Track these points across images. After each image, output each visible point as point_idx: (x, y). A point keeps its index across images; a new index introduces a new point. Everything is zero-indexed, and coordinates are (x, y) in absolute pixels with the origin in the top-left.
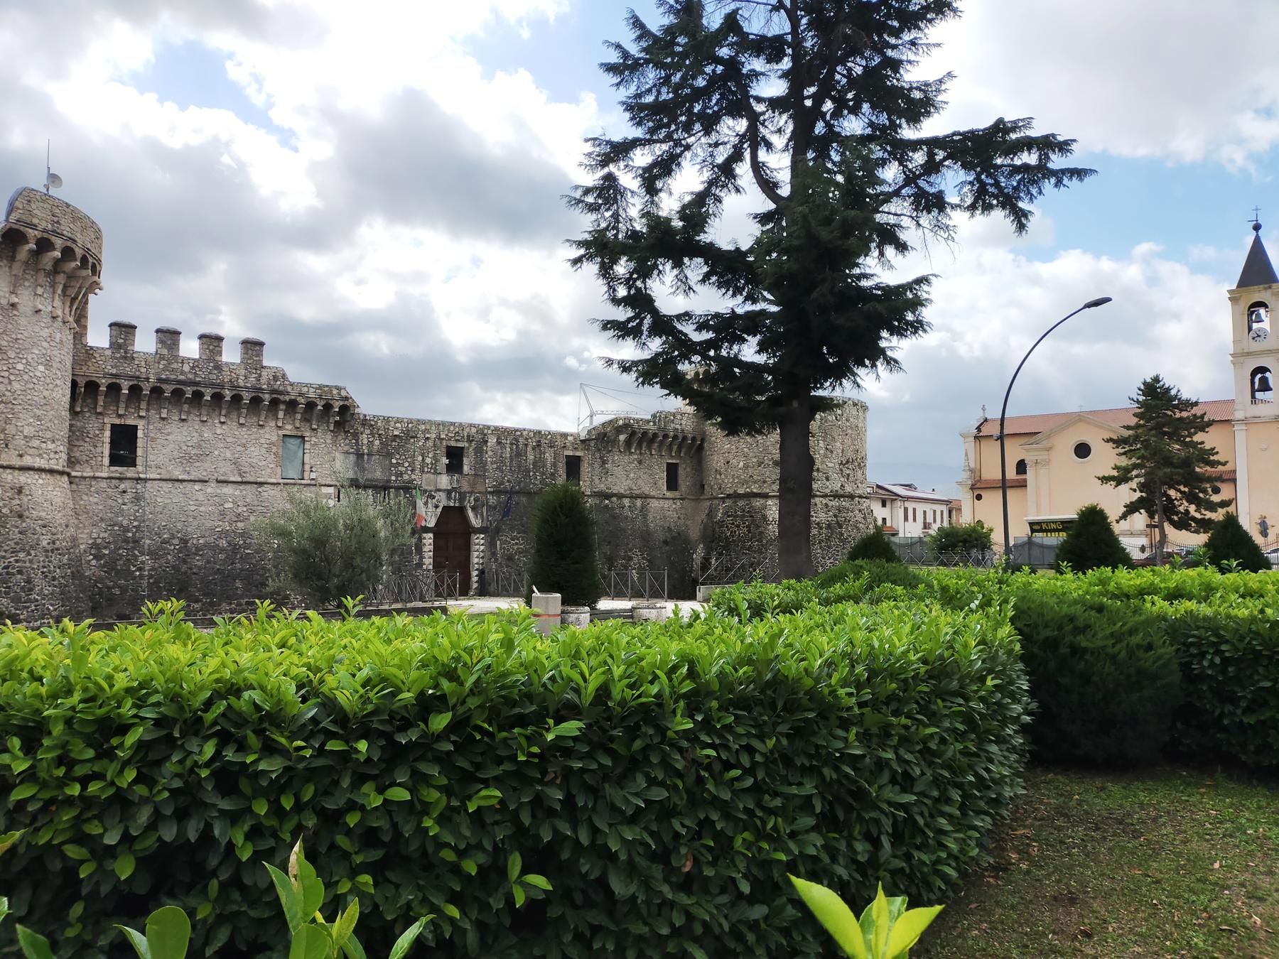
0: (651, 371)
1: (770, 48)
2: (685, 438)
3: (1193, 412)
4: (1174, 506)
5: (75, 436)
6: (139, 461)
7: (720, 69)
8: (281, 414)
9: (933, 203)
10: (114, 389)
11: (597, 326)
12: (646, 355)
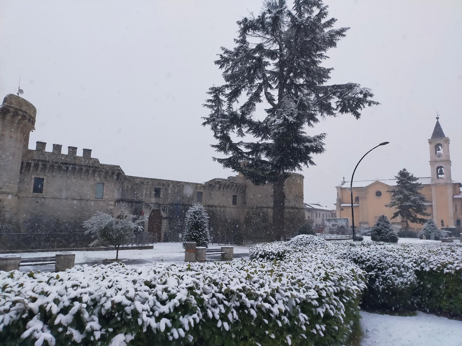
0: (228, 163)
1: (272, 54)
5: (22, 181)
9: (328, 109)
12: (227, 157)
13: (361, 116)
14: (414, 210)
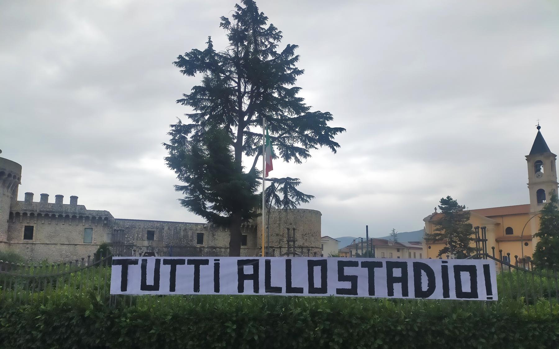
5: (9, 230)
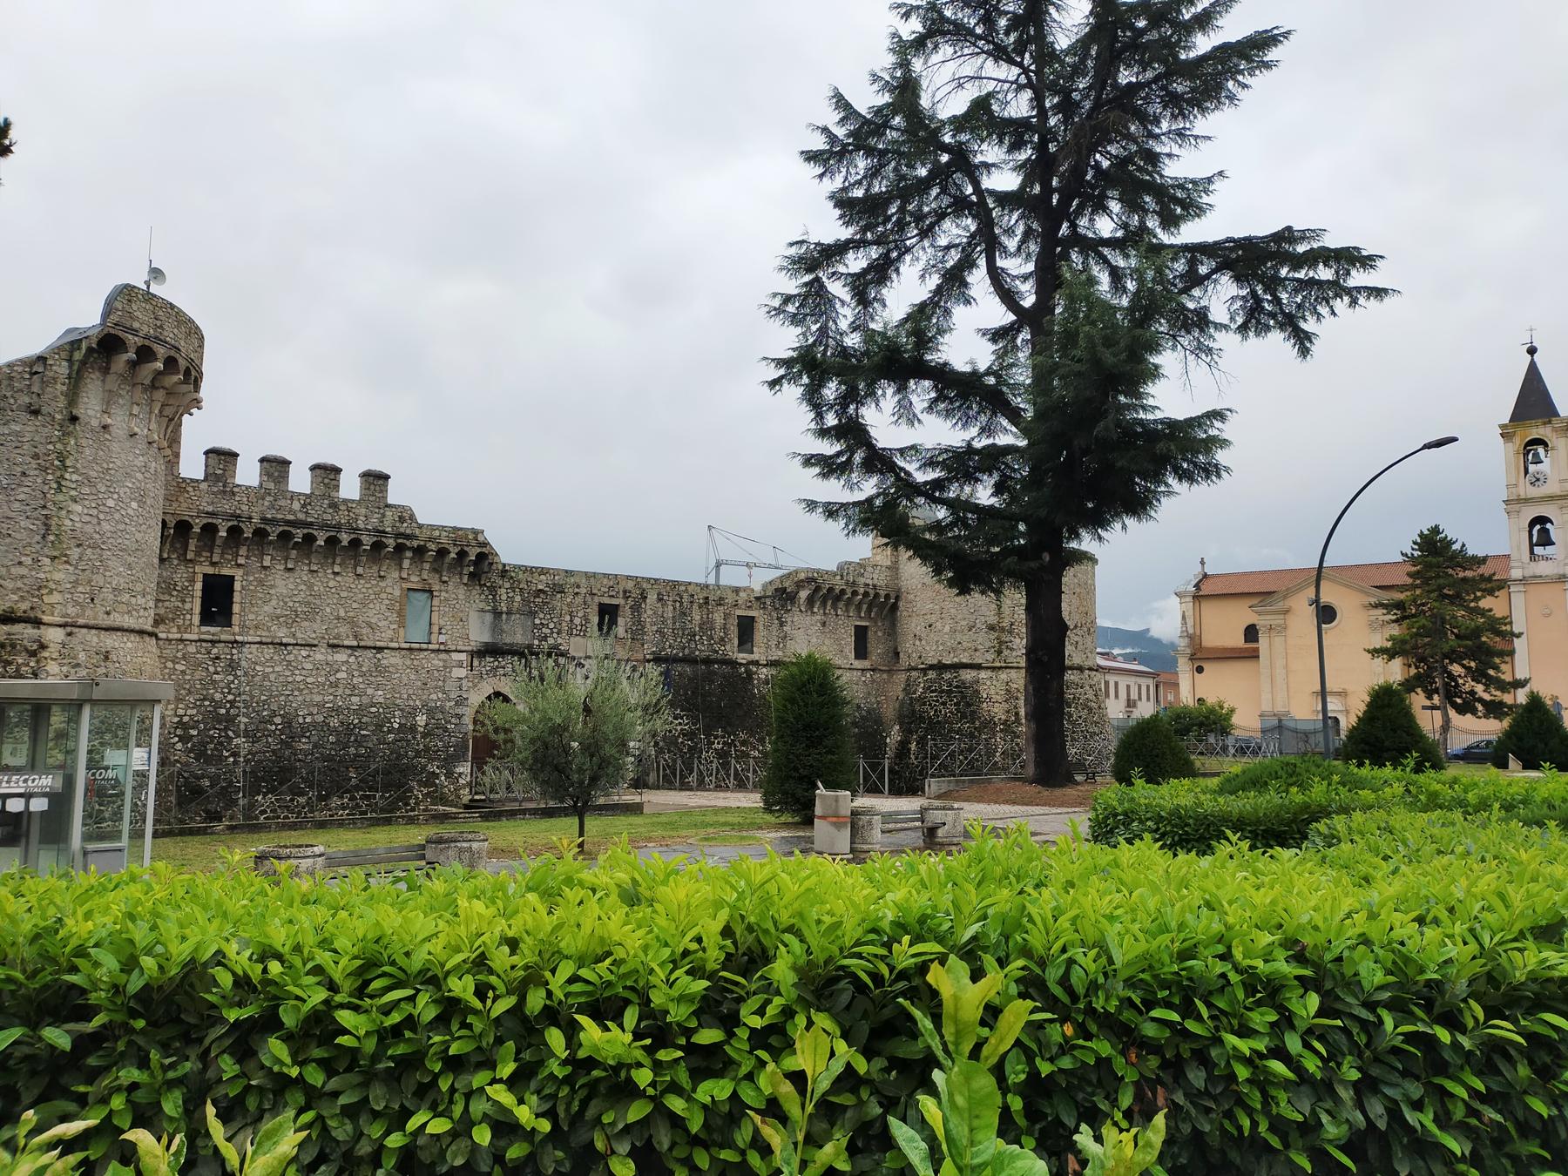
2: (877, 595)
3: (1480, 571)
4: (1457, 685)
6: (235, 619)
7: (945, 158)
8: (406, 563)
10: (210, 529)
11: (798, 461)
13: (1316, 348)
14: (1468, 669)
